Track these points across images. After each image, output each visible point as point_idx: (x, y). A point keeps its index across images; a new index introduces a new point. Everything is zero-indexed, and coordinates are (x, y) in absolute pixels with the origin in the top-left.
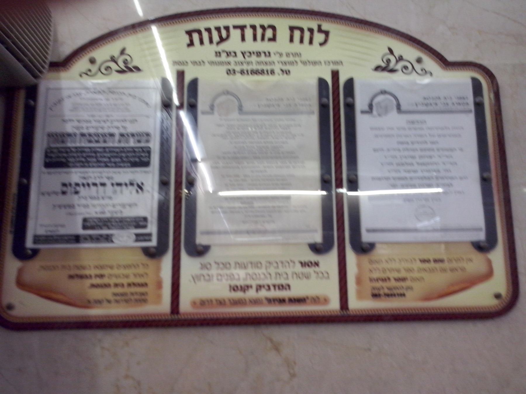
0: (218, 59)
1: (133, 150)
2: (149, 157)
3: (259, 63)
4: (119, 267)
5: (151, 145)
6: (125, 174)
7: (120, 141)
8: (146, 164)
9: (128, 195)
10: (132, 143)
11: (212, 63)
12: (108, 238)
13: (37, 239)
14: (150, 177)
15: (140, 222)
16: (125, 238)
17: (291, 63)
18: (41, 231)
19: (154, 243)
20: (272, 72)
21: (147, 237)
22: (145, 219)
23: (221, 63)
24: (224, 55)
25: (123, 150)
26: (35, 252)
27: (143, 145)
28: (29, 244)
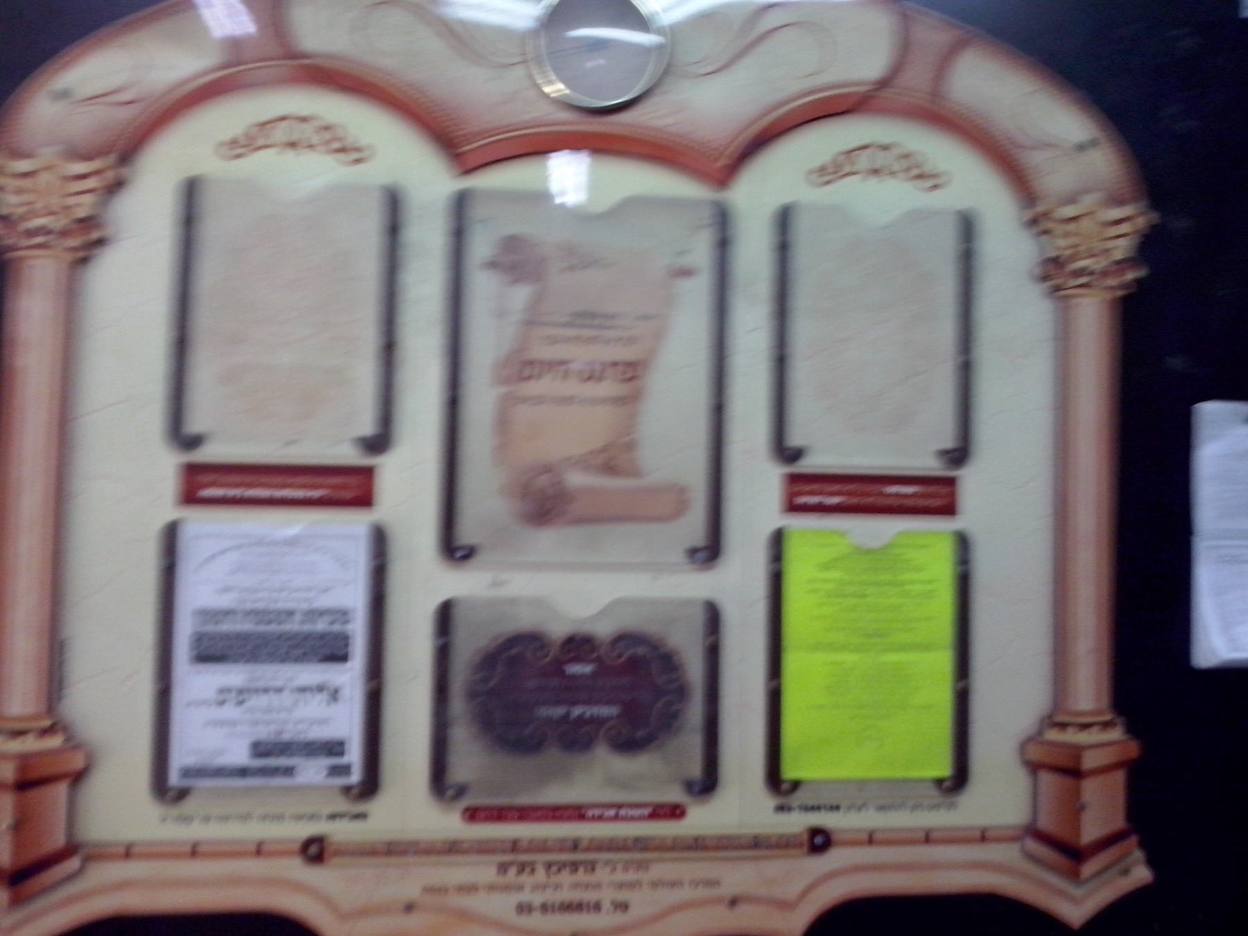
0: (501, 880)
1: (322, 636)
2: (347, 645)
3: (576, 886)
4: (298, 590)
5: (350, 627)
6: (312, 673)
7: (302, 622)
8: (342, 657)
9: (315, 707)
10: (321, 626)
11: (491, 888)
12: (289, 771)
13: (187, 773)
14: (350, 677)
15: (334, 748)
16: (312, 771)
17: (632, 885)
18: (191, 760)
19: (356, 777)
20: (597, 907)
21: (344, 770)
22: (341, 744)
23: (507, 888)
24: (512, 871)
25: (307, 637)
26: (182, 794)
27: (337, 628)
28: (174, 779)
